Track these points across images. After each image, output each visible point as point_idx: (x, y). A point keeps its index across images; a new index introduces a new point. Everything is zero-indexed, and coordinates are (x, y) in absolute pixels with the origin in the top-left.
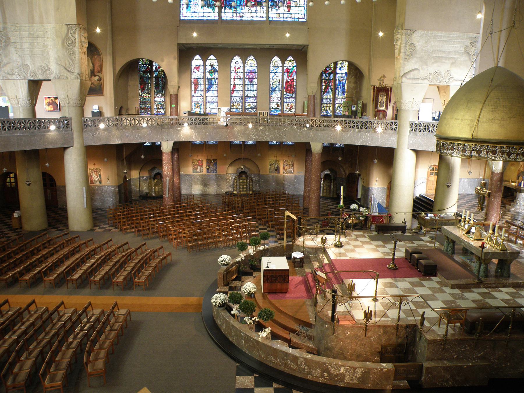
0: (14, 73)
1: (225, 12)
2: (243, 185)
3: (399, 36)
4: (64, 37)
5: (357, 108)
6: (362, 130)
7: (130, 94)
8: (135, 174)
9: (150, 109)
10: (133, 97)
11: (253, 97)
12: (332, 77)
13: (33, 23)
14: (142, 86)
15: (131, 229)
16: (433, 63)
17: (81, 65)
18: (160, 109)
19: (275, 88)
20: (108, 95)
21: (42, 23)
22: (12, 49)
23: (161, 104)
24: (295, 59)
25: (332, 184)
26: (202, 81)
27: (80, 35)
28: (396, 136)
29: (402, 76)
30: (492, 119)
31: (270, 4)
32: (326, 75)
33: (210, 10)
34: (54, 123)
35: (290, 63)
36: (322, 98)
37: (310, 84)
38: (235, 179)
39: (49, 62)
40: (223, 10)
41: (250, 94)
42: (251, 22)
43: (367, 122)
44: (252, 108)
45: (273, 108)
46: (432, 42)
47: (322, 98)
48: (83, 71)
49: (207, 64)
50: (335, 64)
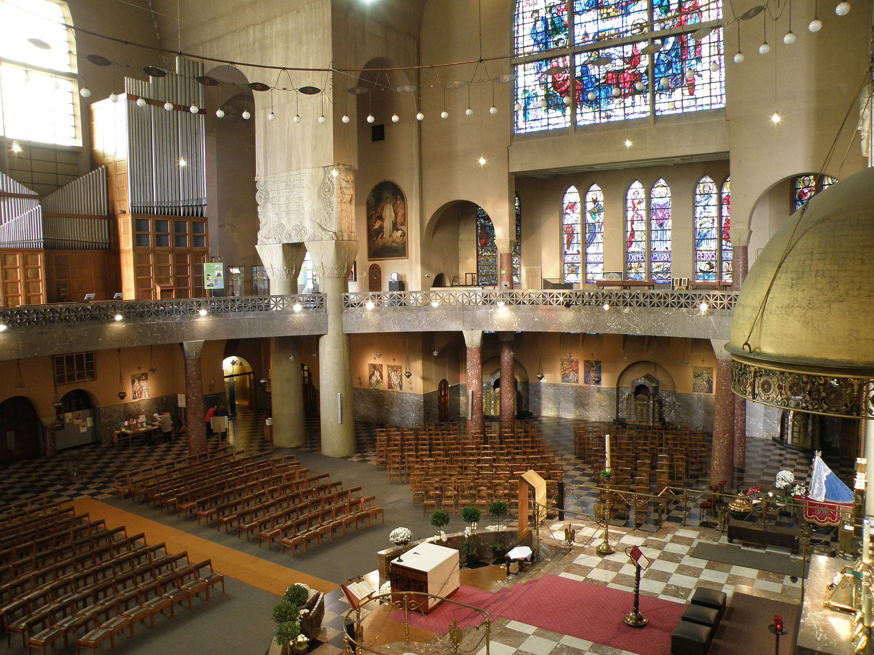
7: (462, 254)
11: (664, 252)
14: (483, 241)
19: (705, 235)
20: (414, 258)
24: (670, 183)
26: (578, 229)
30: (788, 306)
33: (559, 113)
39: (303, 219)
40: (578, 111)
41: (659, 246)
44: (662, 272)
45: (701, 271)
48: (345, 227)
49: (588, 200)
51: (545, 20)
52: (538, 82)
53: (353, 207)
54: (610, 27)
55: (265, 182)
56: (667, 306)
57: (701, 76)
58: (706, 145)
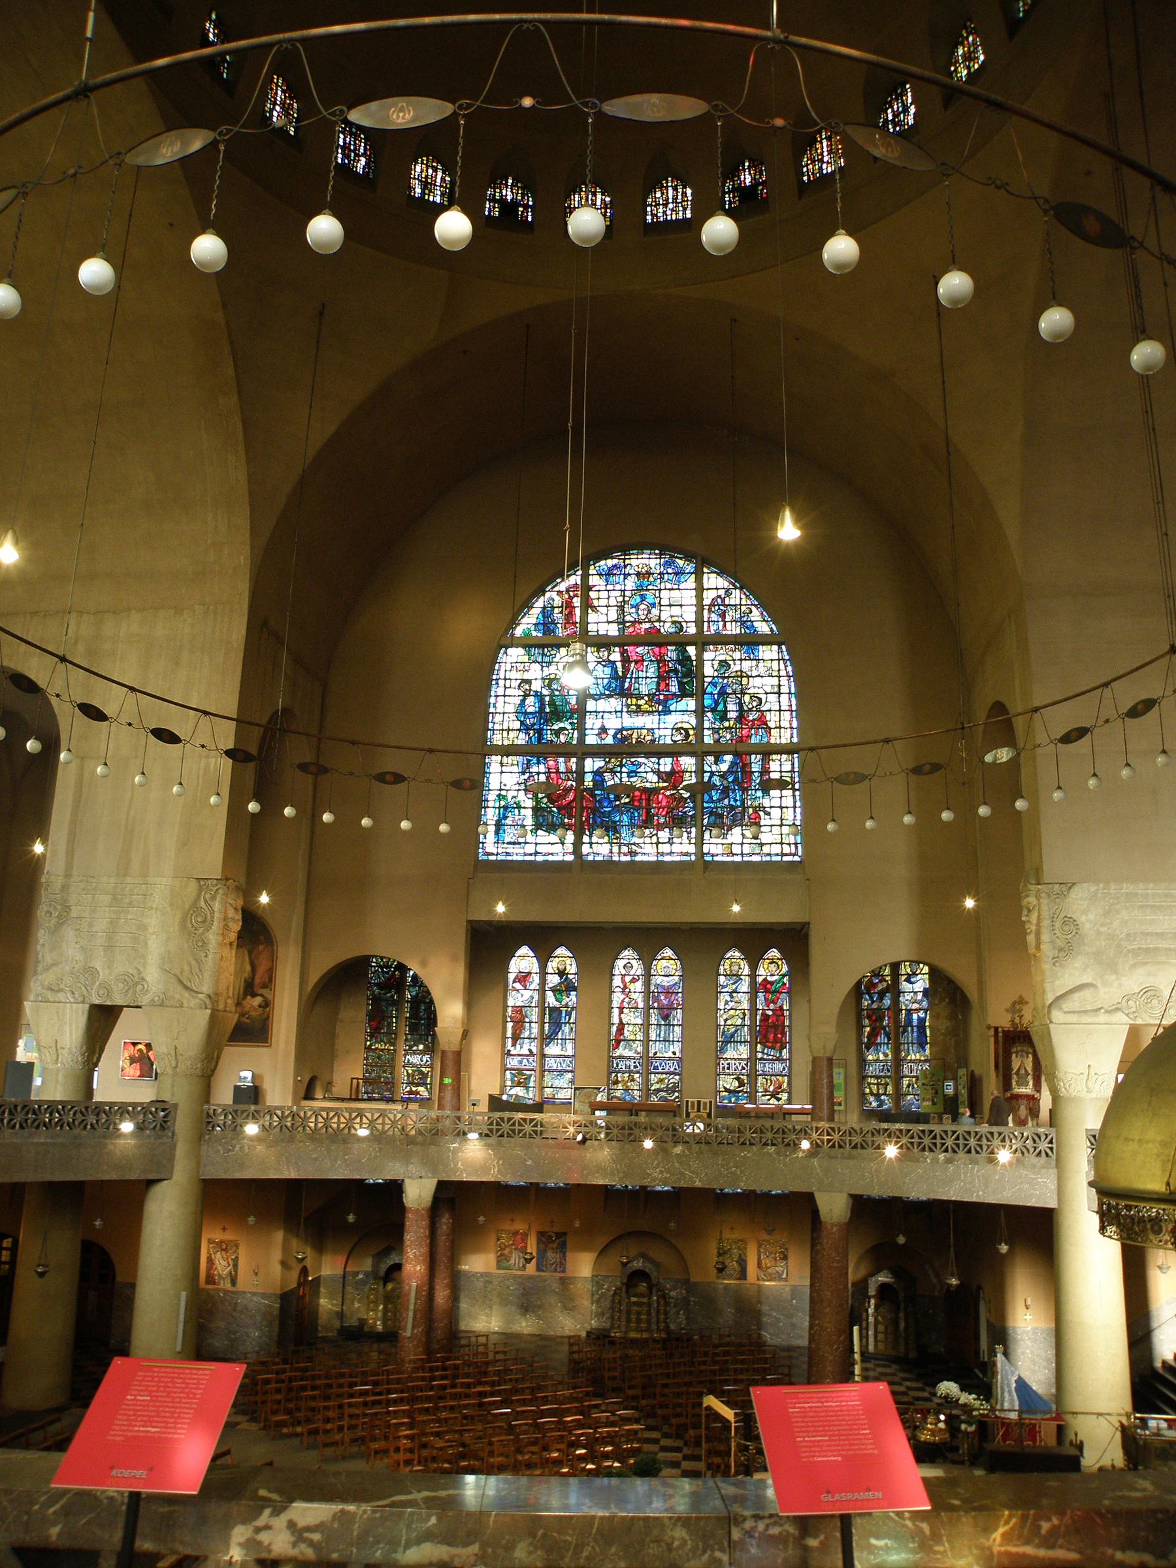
0: (62, 986)
1: (591, 844)
2: (639, 1313)
3: (1032, 900)
4: (187, 907)
5: (956, 1088)
6: (957, 1157)
8: (329, 1267)
9: (391, 1084)
10: (347, 1052)
11: (670, 1059)
12: (887, 1002)
13: (125, 875)
15: (293, 1425)
16: (1134, 966)
17: (218, 973)
18: (418, 1085)
19: (732, 1036)
20: (282, 1046)
21: (144, 875)
22: (69, 933)
23: (421, 1073)
24: (785, 956)
25: (901, 1315)
27: (225, 904)
28: (1053, 1172)
29: (1050, 1006)
31: (705, 821)
32: (871, 998)
34: (132, 1116)
35: (773, 967)
36: (863, 1062)
37: (819, 1024)
38: (615, 1294)
39: (144, 965)
40: (586, 839)
42: (658, 867)
43: (969, 1133)
45: (726, 1090)
46: (1124, 912)
47: (865, 1060)
49: (550, 970)
50: (895, 967)
51: (540, 697)
52: (523, 787)
53: (234, 952)
54: (640, 725)
55: (65, 887)
56: (744, 1144)
57: (769, 814)
58: (782, 911)
